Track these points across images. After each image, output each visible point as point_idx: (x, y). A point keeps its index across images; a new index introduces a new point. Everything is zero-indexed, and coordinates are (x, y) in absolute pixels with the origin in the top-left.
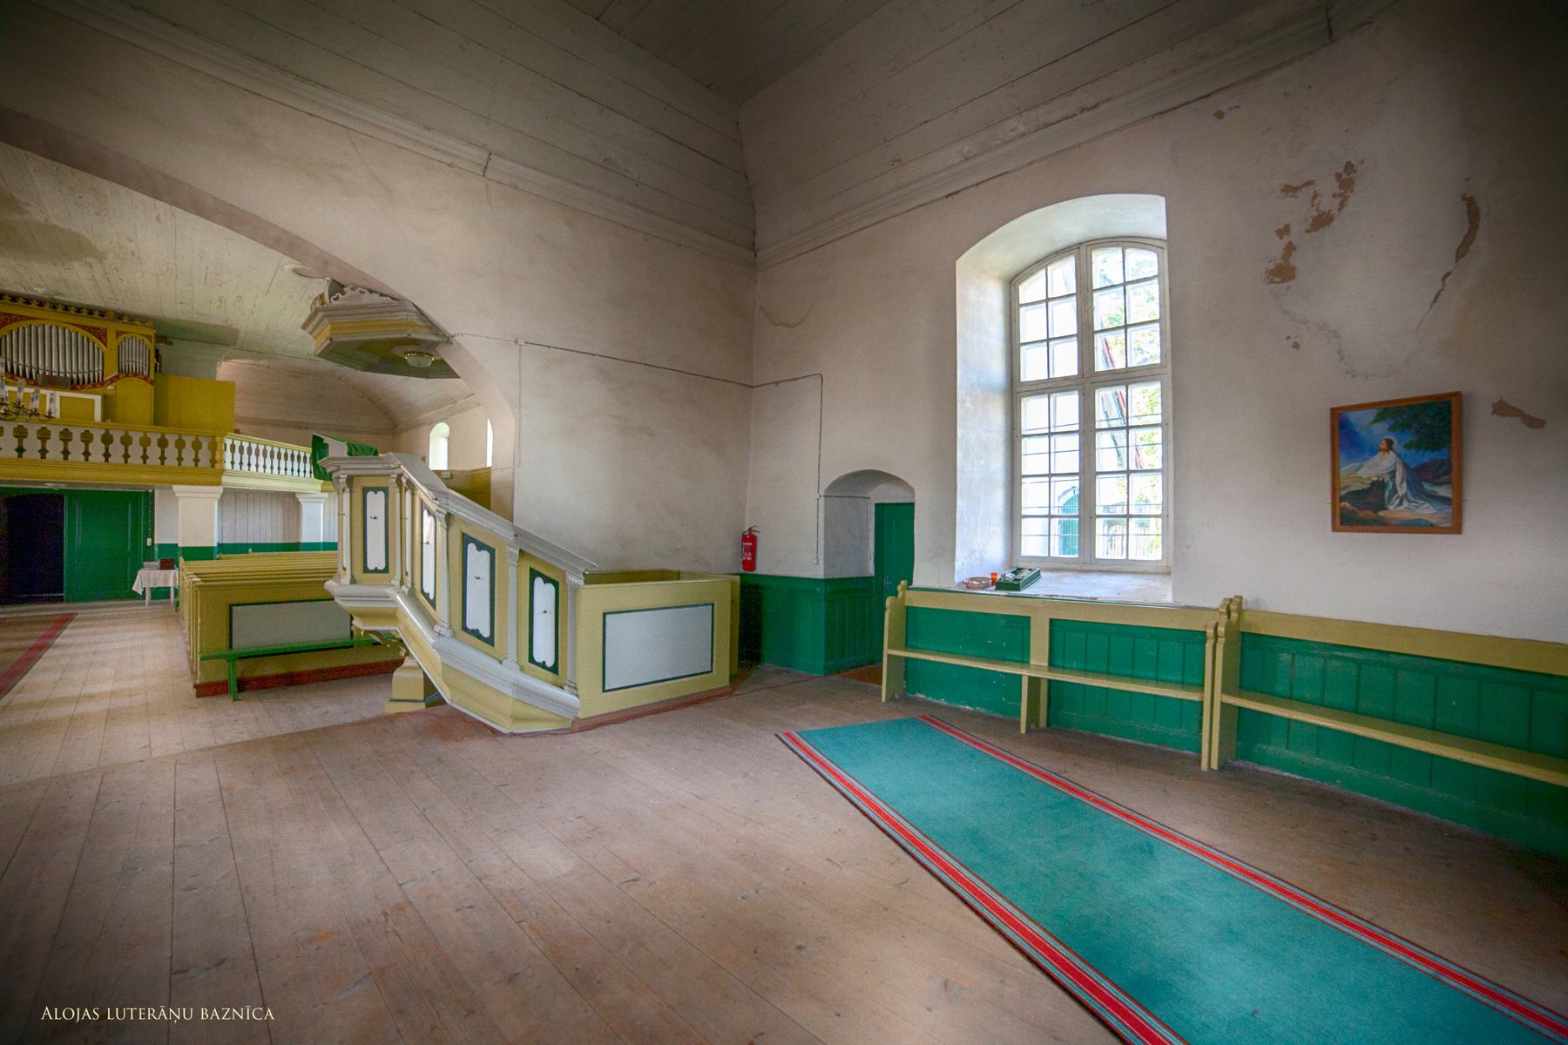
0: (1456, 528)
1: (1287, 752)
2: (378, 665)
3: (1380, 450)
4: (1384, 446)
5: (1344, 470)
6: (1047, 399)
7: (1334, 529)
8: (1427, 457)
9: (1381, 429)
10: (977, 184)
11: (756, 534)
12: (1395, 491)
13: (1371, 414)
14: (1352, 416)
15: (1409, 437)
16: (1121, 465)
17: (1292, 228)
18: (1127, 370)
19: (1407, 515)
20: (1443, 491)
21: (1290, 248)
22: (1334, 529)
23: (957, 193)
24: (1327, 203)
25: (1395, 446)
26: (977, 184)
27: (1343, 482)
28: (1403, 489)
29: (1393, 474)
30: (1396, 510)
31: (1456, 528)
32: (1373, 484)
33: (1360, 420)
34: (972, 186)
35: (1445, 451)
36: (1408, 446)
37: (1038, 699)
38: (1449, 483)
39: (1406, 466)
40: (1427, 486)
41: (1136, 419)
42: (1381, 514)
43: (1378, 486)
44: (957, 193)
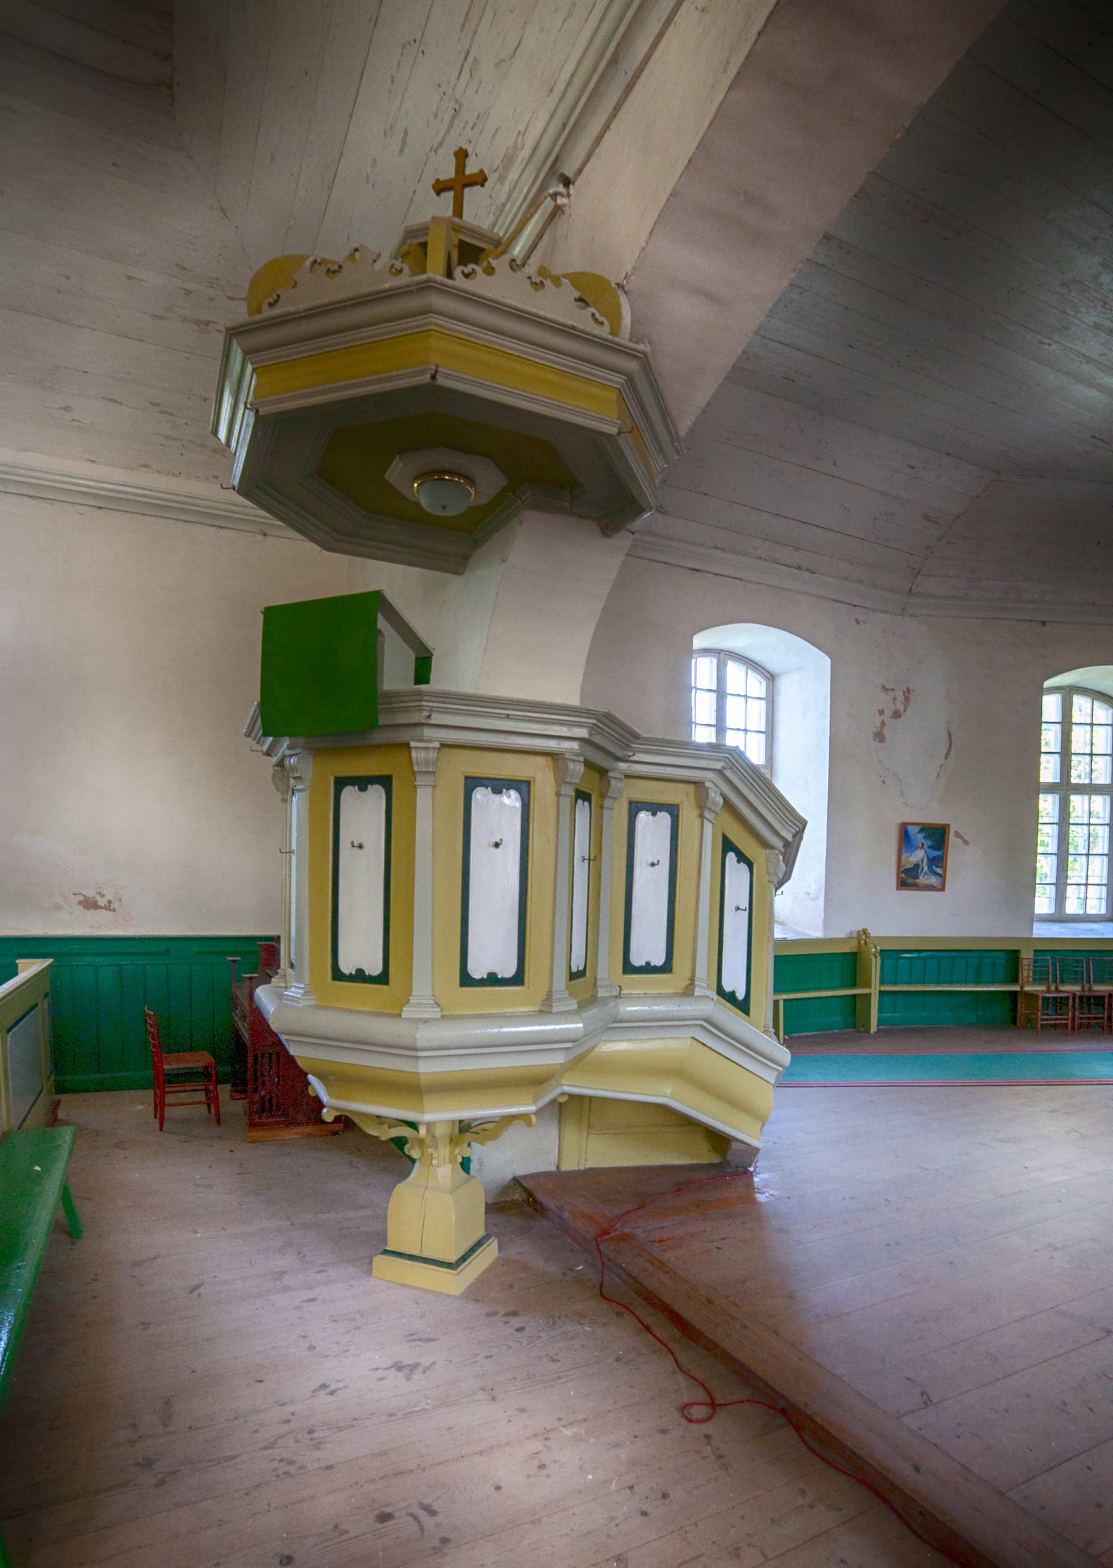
0: (943, 889)
1: (896, 1015)
2: (11, 1030)
3: (918, 848)
4: (920, 846)
5: (904, 856)
6: (1058, 721)
7: (898, 889)
8: (936, 853)
9: (920, 836)
10: (716, 574)
11: (904, 701)
12: (923, 869)
13: (918, 828)
14: (910, 828)
15: (930, 843)
16: (1091, 909)
17: (885, 712)
18: (1071, 723)
19: (927, 882)
20: (939, 871)
21: (883, 724)
22: (898, 889)
23: (698, 571)
24: (900, 707)
25: (925, 847)
26: (716, 574)
27: (903, 863)
28: (926, 869)
29: (923, 860)
30: (922, 880)
31: (943, 889)
32: (915, 865)
33: (913, 830)
34: (712, 573)
35: (942, 851)
36: (930, 847)
37: (778, 1016)
38: (942, 867)
39: (928, 858)
40: (934, 868)
41: (1096, 819)
42: (917, 881)
43: (917, 866)
44: (698, 571)
